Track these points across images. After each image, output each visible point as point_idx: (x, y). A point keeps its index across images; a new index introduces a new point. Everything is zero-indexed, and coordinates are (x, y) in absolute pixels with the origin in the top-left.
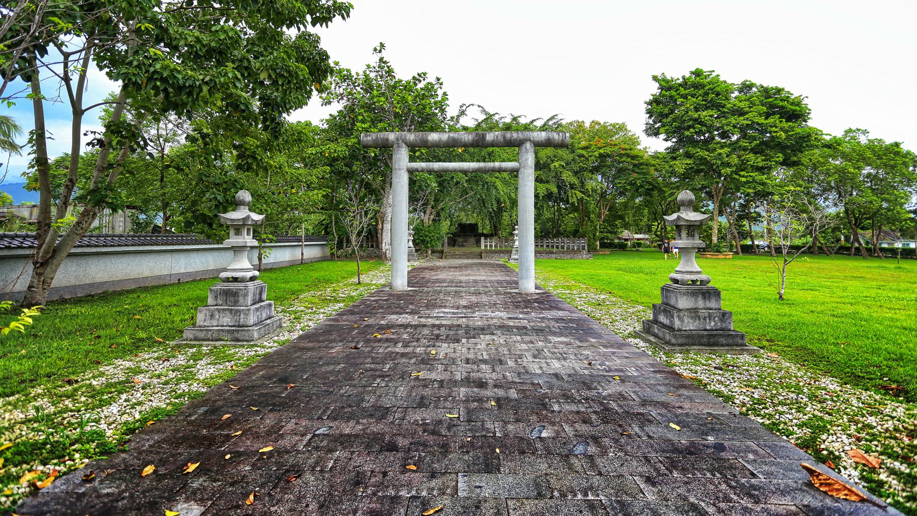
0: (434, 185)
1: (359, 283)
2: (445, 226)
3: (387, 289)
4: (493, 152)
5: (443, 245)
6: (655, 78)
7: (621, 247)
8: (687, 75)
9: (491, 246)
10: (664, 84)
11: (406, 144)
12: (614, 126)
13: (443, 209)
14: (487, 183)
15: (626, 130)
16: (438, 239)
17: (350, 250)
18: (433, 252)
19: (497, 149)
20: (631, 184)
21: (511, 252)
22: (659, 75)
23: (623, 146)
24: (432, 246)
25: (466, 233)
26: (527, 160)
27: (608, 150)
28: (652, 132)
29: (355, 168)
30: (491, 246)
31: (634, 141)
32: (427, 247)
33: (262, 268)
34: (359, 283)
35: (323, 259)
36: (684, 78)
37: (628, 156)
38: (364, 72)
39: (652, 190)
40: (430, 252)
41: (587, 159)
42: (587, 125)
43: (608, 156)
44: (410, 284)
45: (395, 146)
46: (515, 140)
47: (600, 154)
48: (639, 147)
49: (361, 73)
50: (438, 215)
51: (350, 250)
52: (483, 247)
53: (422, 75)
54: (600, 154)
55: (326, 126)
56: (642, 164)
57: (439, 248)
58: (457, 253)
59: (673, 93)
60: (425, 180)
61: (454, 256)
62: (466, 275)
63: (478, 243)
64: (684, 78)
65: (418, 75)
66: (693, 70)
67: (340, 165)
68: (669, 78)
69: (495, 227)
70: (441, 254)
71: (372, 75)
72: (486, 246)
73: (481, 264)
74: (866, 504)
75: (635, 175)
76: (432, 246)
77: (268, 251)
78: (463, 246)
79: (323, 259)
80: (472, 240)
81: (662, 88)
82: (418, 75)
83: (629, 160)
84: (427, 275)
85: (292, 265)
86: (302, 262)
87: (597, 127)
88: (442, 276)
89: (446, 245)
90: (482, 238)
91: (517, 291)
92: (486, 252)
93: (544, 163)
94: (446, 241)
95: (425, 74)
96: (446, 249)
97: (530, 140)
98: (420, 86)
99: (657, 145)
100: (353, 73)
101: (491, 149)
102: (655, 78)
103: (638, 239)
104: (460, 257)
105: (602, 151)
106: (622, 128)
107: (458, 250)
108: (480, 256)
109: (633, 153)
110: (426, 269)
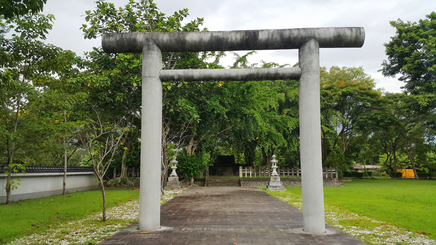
0: (196, 116)
1: (104, 220)
2: (206, 157)
3: (134, 230)
4: (251, 86)
5: (204, 174)
6: (393, 24)
7: (357, 176)
8: (424, 18)
9: (248, 174)
10: (402, 28)
11: (158, 45)
12: (352, 70)
13: (204, 141)
14: (245, 115)
15: (363, 73)
16: (201, 168)
17: (119, 179)
18: (195, 180)
19: (255, 82)
20: (372, 119)
21: (269, 180)
22: (395, 20)
23: (361, 86)
24: (195, 175)
25: (223, 167)
26: (310, 62)
27: (350, 89)
28: (390, 71)
29: (118, 98)
30: (248, 174)
31: (370, 83)
32: (191, 176)
33: (10, 199)
34: (104, 220)
35: (92, 189)
36: (421, 21)
37: (368, 95)
38: (128, 8)
39: (390, 124)
40: (193, 180)
41: (331, 98)
42: (328, 71)
43: (351, 94)
44: (165, 218)
45: (145, 49)
46: (296, 38)
47: (343, 93)
48: (374, 89)
49: (124, 8)
50: (200, 145)
51: (119, 179)
52: (241, 176)
53: (184, 13)
54: (343, 93)
55: (90, 60)
56: (379, 102)
57: (201, 177)
58: (218, 181)
59: (413, 34)
60: (187, 112)
61: (215, 184)
62: (231, 206)
63: (236, 172)
64: (421, 21)
65: (180, 12)
66: (429, 14)
67: (104, 96)
68: (405, 22)
69: (249, 158)
70: (203, 183)
71: (135, 10)
72: (244, 174)
73: (242, 192)
74: (250, 211)
75: (376, 111)
76: (195, 175)
77: (16, 181)
78: (222, 175)
79: (92, 189)
80: (230, 170)
81: (400, 32)
82: (180, 12)
83: (369, 98)
84: (188, 205)
85: (54, 196)
86: (65, 192)
87: (337, 72)
88: (204, 206)
89: (207, 174)
90: (241, 168)
91: (299, 231)
92: (245, 180)
93: (293, 102)
94: (207, 169)
95: (186, 10)
96: (208, 177)
97: (314, 38)
98: (184, 23)
99: (393, 86)
100: (117, 8)
101: (249, 83)
102: (393, 24)
103: (368, 169)
104: (221, 184)
105: (345, 90)
106: (358, 72)
107: (218, 179)
108: (239, 183)
109: (371, 92)
110: (187, 197)
